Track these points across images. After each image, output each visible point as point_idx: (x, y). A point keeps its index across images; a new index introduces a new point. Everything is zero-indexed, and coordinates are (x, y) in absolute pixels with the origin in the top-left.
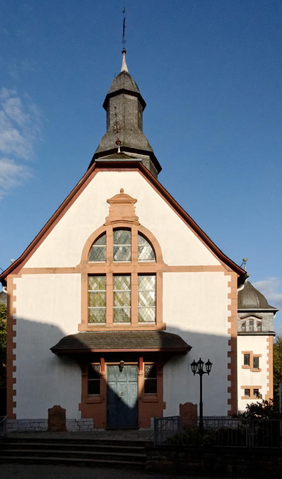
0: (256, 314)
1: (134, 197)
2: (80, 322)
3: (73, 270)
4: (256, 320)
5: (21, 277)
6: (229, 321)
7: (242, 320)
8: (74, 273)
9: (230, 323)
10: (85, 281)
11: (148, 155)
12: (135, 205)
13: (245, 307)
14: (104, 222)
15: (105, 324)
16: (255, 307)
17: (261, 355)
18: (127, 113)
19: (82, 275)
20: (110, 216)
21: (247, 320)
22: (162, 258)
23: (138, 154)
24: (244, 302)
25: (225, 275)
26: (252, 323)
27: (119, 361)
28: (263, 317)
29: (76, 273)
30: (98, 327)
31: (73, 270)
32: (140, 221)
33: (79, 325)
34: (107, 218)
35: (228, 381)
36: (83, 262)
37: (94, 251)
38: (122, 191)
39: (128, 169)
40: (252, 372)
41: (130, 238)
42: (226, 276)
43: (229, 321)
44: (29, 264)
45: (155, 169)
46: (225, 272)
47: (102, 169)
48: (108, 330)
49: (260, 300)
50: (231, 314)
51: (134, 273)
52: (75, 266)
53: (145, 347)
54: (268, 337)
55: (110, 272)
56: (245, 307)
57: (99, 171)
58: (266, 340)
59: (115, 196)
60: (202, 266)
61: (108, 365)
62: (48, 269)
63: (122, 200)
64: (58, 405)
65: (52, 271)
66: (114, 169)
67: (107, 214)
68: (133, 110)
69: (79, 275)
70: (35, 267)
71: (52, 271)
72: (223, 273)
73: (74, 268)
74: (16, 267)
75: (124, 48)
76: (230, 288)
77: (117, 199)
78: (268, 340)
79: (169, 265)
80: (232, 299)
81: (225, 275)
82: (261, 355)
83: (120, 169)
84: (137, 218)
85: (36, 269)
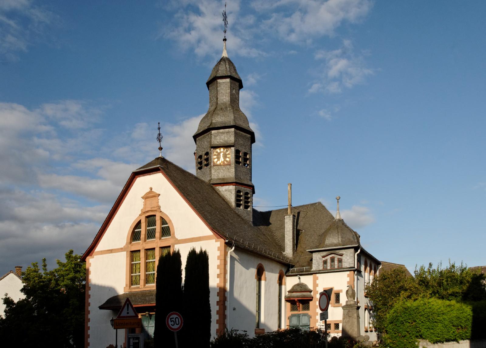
0: (337, 251)
1: (158, 193)
2: (125, 286)
3: (121, 250)
4: (337, 257)
5: (93, 258)
6: (218, 277)
7: (323, 258)
8: (122, 251)
9: (218, 279)
10: (128, 256)
11: (233, 128)
12: (159, 198)
13: (327, 246)
14: (140, 213)
15: (139, 286)
16: (336, 245)
17: (341, 291)
18: (221, 95)
19: (127, 253)
20: (145, 208)
21: (328, 258)
22: (174, 234)
23: (224, 130)
24: (326, 241)
25: (216, 241)
26: (332, 260)
27: (145, 312)
28: (343, 254)
29: (123, 251)
30: (135, 289)
31: (121, 250)
32: (162, 209)
33: (124, 288)
34: (142, 210)
35: (217, 325)
36: (127, 243)
37: (135, 236)
38: (151, 189)
39: (155, 172)
40: (333, 308)
41: (19, 268)
42: (217, 243)
43: (218, 277)
44: (99, 248)
45: (245, 136)
46: (215, 239)
47: (139, 176)
48: (140, 290)
49: (342, 237)
50: (219, 272)
51: (157, 247)
52: (123, 247)
53: (151, 303)
54: (348, 272)
55: (143, 249)
56: (327, 246)
57: (137, 178)
58: (347, 276)
59: (147, 193)
60: (200, 237)
61: (141, 315)
62: (108, 250)
63: (151, 196)
64: (112, 344)
65: (110, 252)
66: (147, 174)
67: (142, 207)
68: (226, 90)
69: (125, 252)
70: (101, 250)
71: (110, 252)
72: (214, 240)
73: (122, 248)
74: (90, 251)
75: (225, 37)
76: (219, 252)
77: (148, 196)
78: (348, 276)
79: (179, 239)
80: (220, 260)
81: (216, 241)
82: (341, 291)
83: (150, 173)
84: (159, 207)
85: (101, 251)
